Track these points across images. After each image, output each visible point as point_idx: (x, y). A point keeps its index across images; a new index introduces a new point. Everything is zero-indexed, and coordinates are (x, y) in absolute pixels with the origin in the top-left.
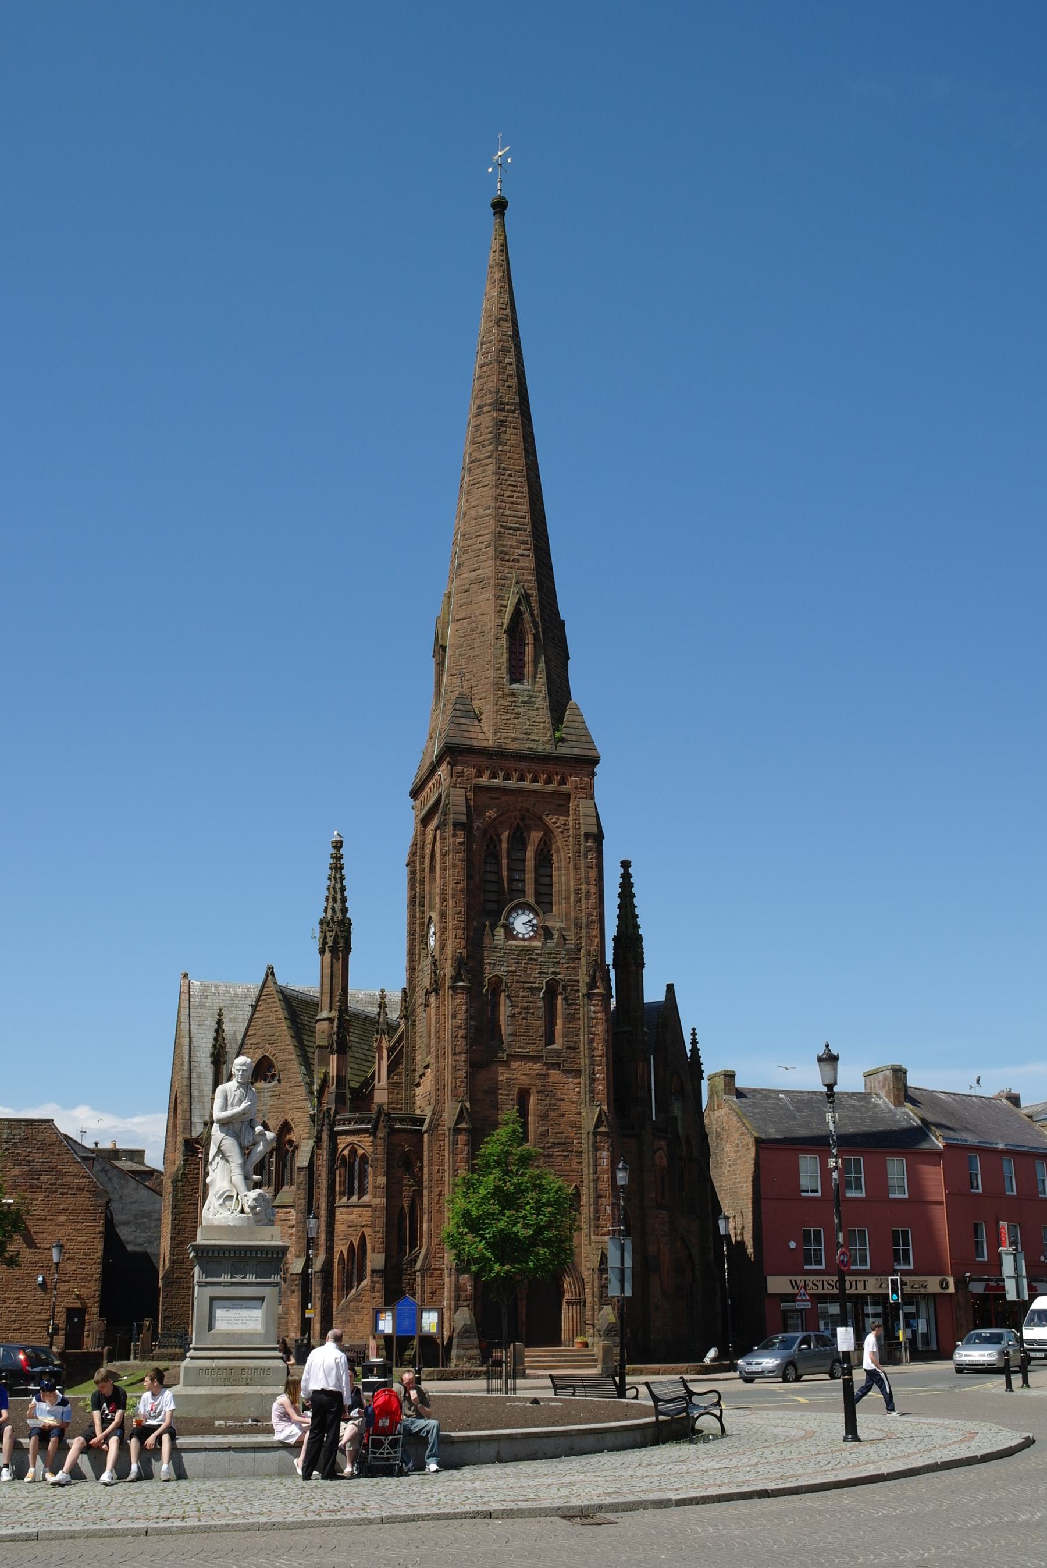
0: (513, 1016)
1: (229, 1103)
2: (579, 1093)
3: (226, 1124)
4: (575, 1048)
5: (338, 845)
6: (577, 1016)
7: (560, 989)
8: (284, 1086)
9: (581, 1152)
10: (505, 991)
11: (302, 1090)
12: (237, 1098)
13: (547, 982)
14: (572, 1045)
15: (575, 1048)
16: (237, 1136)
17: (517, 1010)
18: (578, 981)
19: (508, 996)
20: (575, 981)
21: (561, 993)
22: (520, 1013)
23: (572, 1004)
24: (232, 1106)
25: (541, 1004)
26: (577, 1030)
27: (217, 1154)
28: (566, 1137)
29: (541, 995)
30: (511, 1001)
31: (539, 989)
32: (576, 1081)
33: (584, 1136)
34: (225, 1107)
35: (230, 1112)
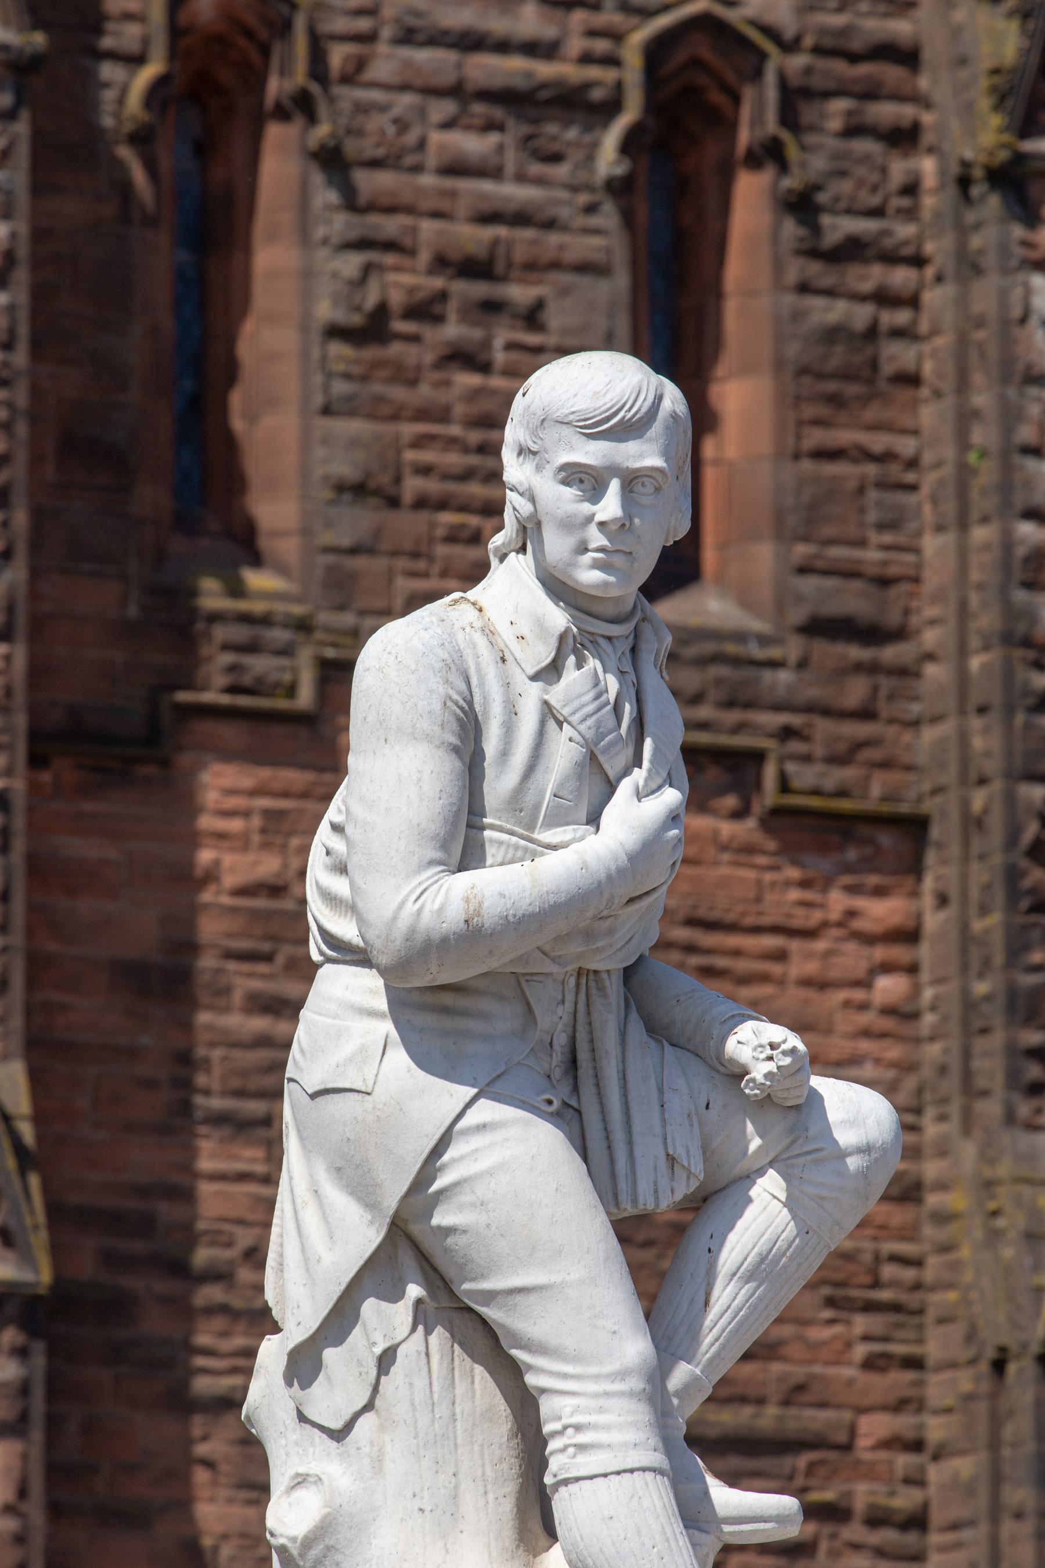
0: (371, 329)
1: (499, 785)
2: (903, 1013)
3: (449, 1000)
4: (872, 634)
6: (898, 355)
7: (756, 116)
9: (917, 1521)
10: (303, 106)
12: (564, 752)
13: (657, 51)
14: (852, 601)
15: (872, 634)
16: (572, 1095)
17: (402, 282)
18: (908, 57)
19: (332, 160)
20: (889, 52)
21: (770, 154)
22: (426, 310)
23: (853, 250)
24: (523, 812)
25: (603, 235)
26: (897, 474)
27: (376, 1276)
28: (796, 1393)
29: (608, 156)
30: (351, 203)
31: (612, 107)
32: (883, 911)
33: (938, 1388)
34: (463, 842)
35: (508, 882)
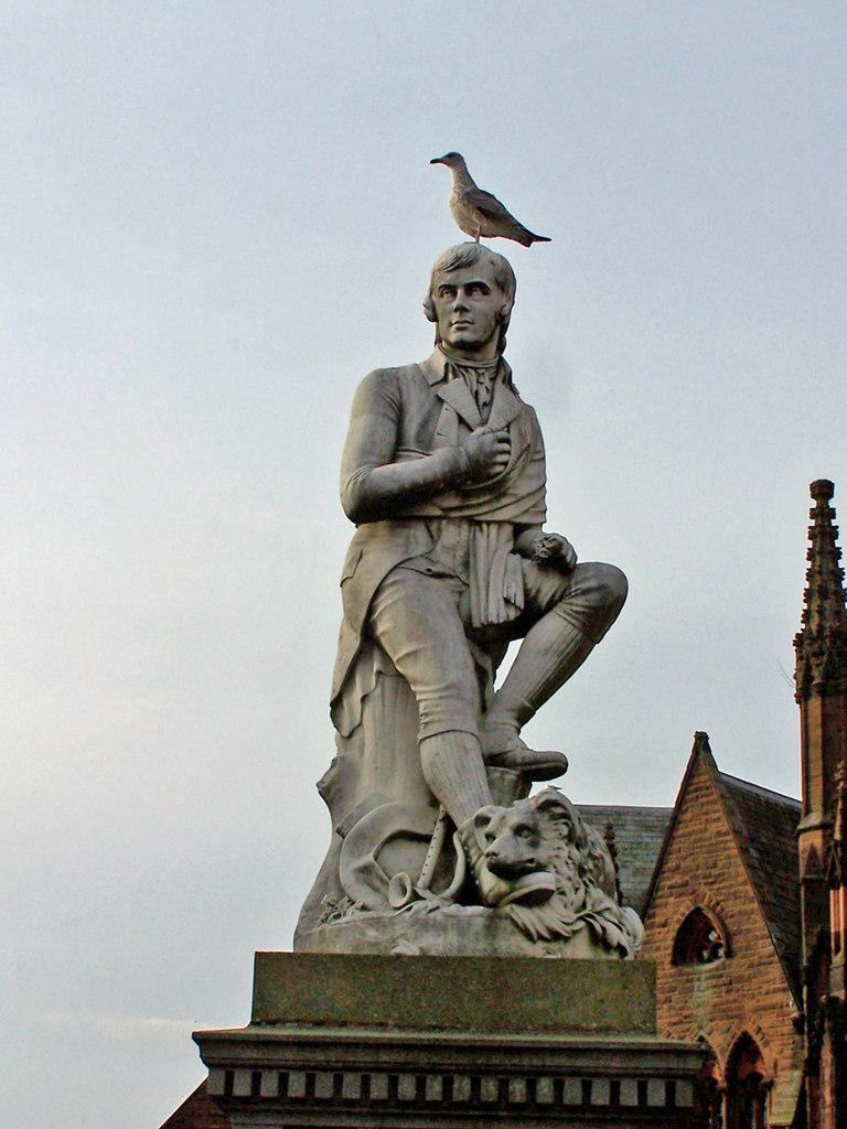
5: (823, 490)
8: (739, 966)
11: (776, 971)
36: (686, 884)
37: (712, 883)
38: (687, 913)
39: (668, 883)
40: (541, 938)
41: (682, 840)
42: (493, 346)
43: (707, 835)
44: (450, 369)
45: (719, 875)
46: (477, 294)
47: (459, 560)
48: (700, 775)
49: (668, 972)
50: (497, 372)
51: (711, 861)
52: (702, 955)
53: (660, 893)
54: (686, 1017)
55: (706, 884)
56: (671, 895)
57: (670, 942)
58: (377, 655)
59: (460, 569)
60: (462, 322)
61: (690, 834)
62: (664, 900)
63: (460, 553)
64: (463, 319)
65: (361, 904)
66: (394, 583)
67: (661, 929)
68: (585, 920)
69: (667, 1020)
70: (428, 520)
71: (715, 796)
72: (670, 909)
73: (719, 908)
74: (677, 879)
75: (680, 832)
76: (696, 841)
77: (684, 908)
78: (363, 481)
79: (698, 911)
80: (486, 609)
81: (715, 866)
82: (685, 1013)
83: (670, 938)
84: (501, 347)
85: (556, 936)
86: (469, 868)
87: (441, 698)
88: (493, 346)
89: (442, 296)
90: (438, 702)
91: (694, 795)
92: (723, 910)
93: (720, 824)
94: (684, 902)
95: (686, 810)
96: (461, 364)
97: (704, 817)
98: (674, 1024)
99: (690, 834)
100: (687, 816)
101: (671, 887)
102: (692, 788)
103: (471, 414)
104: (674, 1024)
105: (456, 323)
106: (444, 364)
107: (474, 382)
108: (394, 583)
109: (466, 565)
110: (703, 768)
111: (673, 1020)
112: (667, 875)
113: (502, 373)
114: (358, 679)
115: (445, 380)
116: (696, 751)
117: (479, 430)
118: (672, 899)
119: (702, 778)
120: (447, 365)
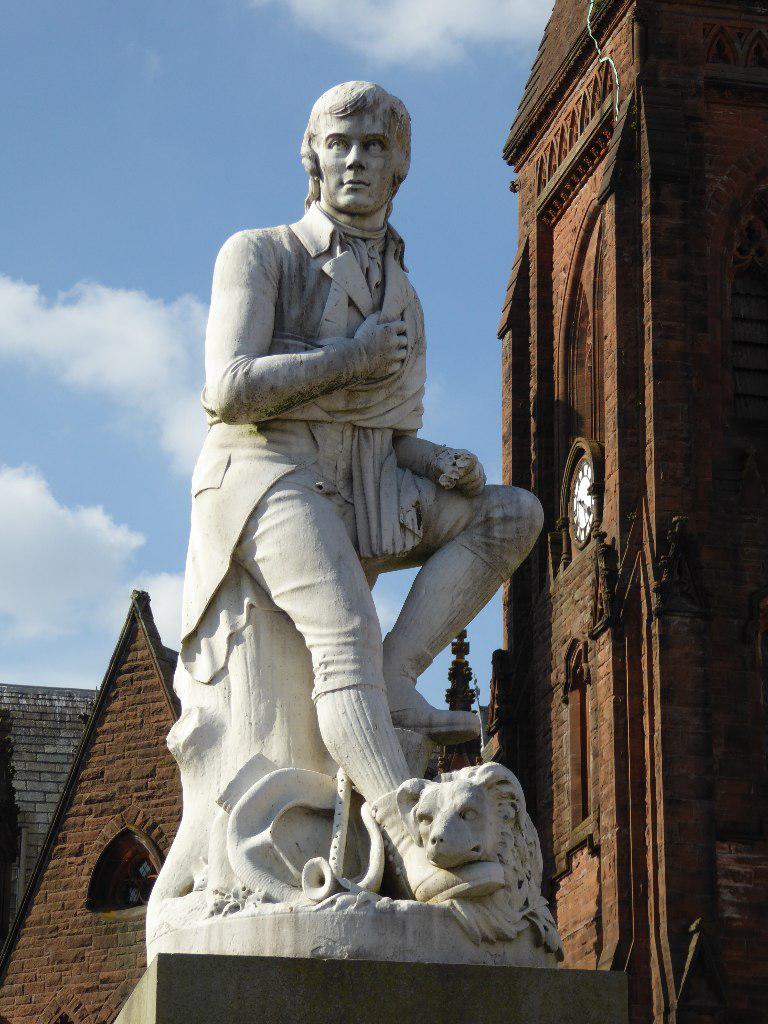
36: (109, 799)
37: (150, 797)
38: (111, 838)
39: (87, 796)
40: (485, 939)
41: (110, 737)
42: (383, 212)
43: (146, 730)
44: (338, 238)
45: (159, 787)
46: (375, 149)
47: (340, 474)
48: (136, 650)
49: (80, 919)
50: (386, 245)
51: (149, 768)
52: (128, 895)
53: (73, 809)
54: (104, 981)
55: (139, 798)
56: (91, 812)
57: (86, 879)
58: (246, 583)
59: (341, 484)
60: (359, 182)
61: (120, 730)
62: (79, 819)
63: (342, 465)
64: (360, 178)
65: (263, 893)
66: (279, 500)
67: (73, 859)
68: (528, 920)
69: (75, 986)
70: (311, 424)
71: (156, 680)
72: (87, 832)
73: (156, 831)
74: (98, 792)
75: (106, 726)
76: (128, 740)
77: (110, 830)
78: (247, 373)
79: (126, 835)
80: (380, 536)
81: (152, 775)
82: (104, 975)
83: (86, 871)
84: (389, 211)
85: (503, 938)
86: (389, 852)
87: (346, 644)
88: (383, 212)
89: (330, 147)
90: (341, 648)
91: (128, 676)
92: (161, 834)
93: (163, 717)
94: (105, 822)
95: (115, 697)
96: (349, 232)
97: (140, 707)
98: (87, 990)
99: (120, 730)
100: (116, 705)
101: (90, 801)
102: (125, 667)
103: (364, 300)
104: (87, 990)
105: (350, 182)
106: (330, 231)
107: (366, 258)
108: (279, 500)
109: (350, 479)
110: (142, 639)
111: (85, 985)
112: (83, 784)
113: (392, 246)
114: (223, 616)
115: (330, 252)
116: (132, 619)
117: (372, 319)
118: (90, 818)
119: (140, 654)
120: (333, 235)
